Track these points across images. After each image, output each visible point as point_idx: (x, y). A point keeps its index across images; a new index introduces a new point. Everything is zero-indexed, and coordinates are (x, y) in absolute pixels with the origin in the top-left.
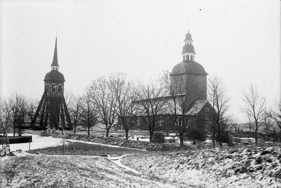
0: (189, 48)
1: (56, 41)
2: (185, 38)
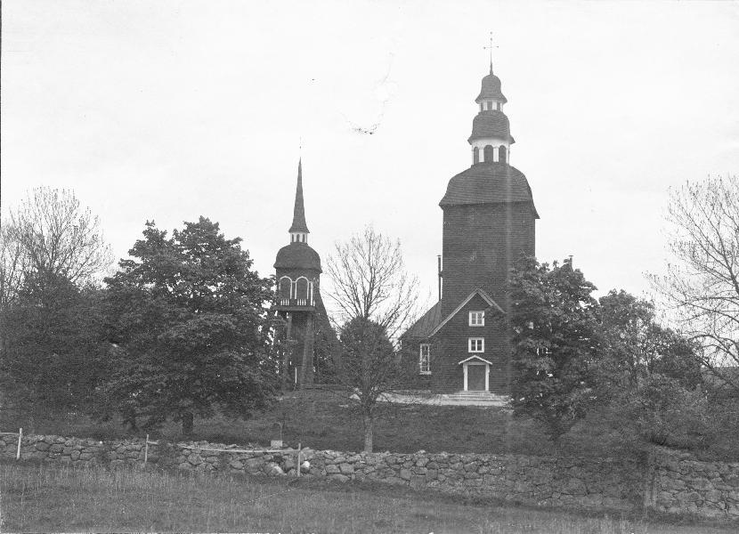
0: (491, 125)
1: (300, 179)
2: (478, 91)
